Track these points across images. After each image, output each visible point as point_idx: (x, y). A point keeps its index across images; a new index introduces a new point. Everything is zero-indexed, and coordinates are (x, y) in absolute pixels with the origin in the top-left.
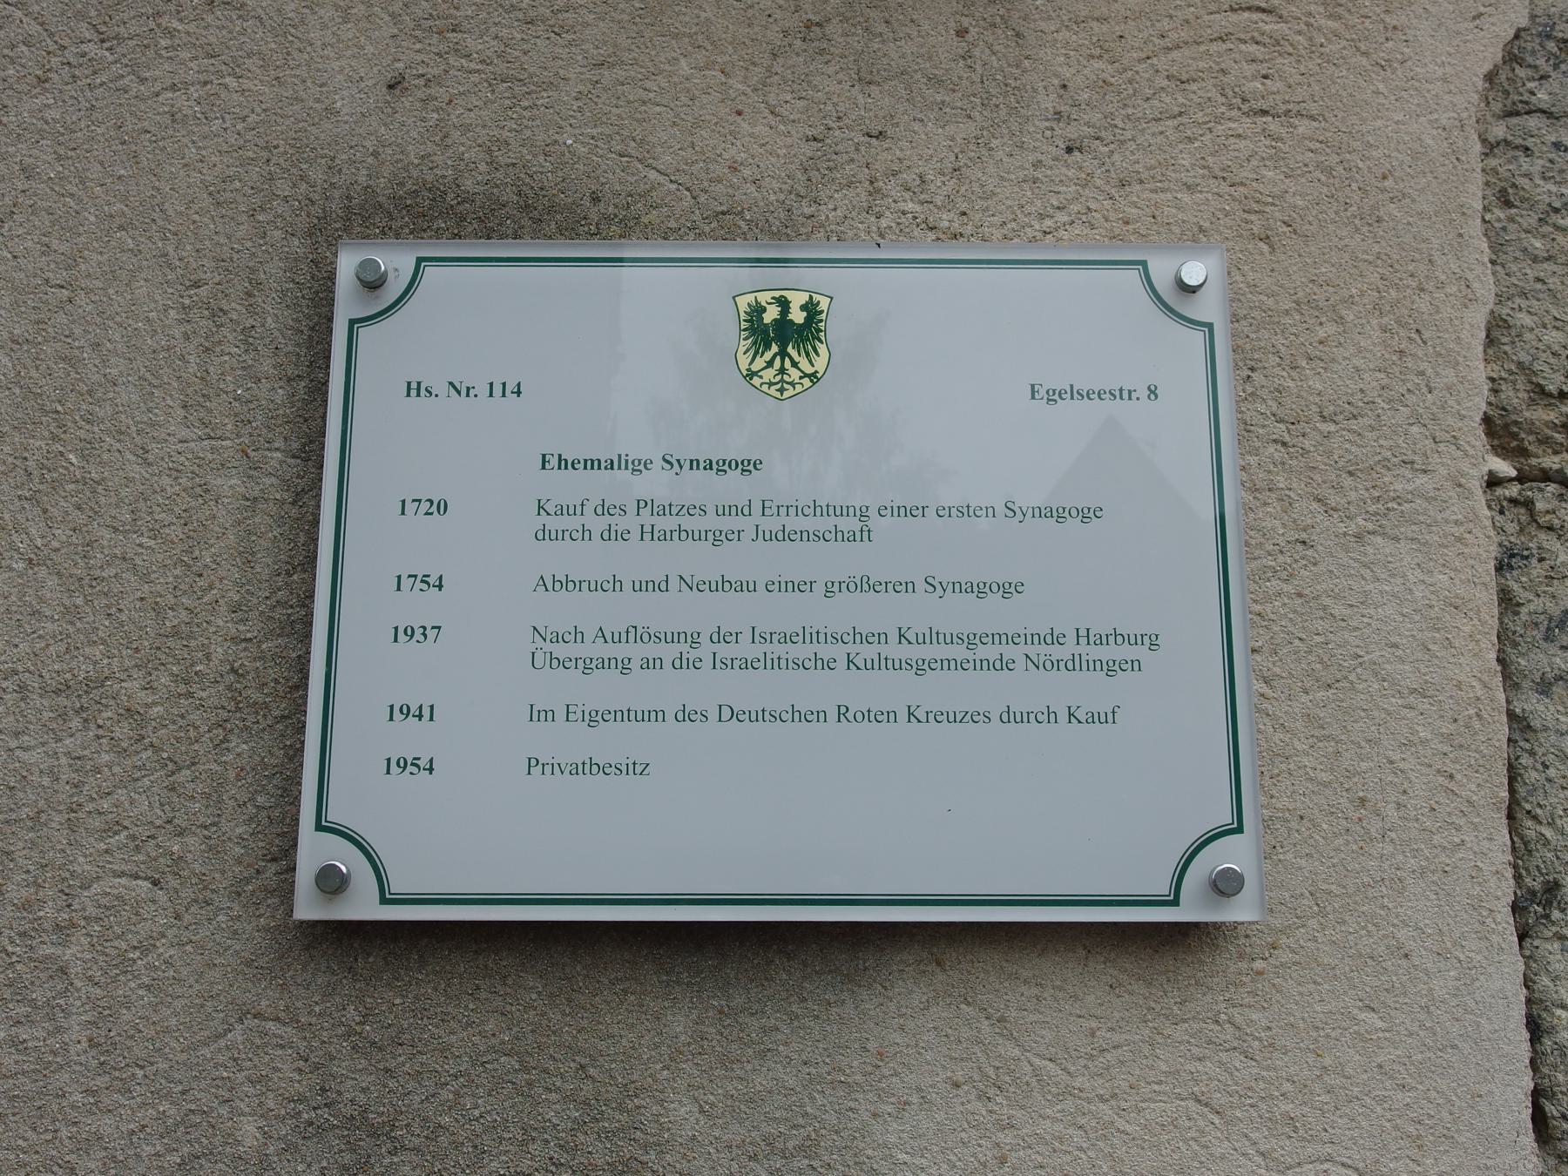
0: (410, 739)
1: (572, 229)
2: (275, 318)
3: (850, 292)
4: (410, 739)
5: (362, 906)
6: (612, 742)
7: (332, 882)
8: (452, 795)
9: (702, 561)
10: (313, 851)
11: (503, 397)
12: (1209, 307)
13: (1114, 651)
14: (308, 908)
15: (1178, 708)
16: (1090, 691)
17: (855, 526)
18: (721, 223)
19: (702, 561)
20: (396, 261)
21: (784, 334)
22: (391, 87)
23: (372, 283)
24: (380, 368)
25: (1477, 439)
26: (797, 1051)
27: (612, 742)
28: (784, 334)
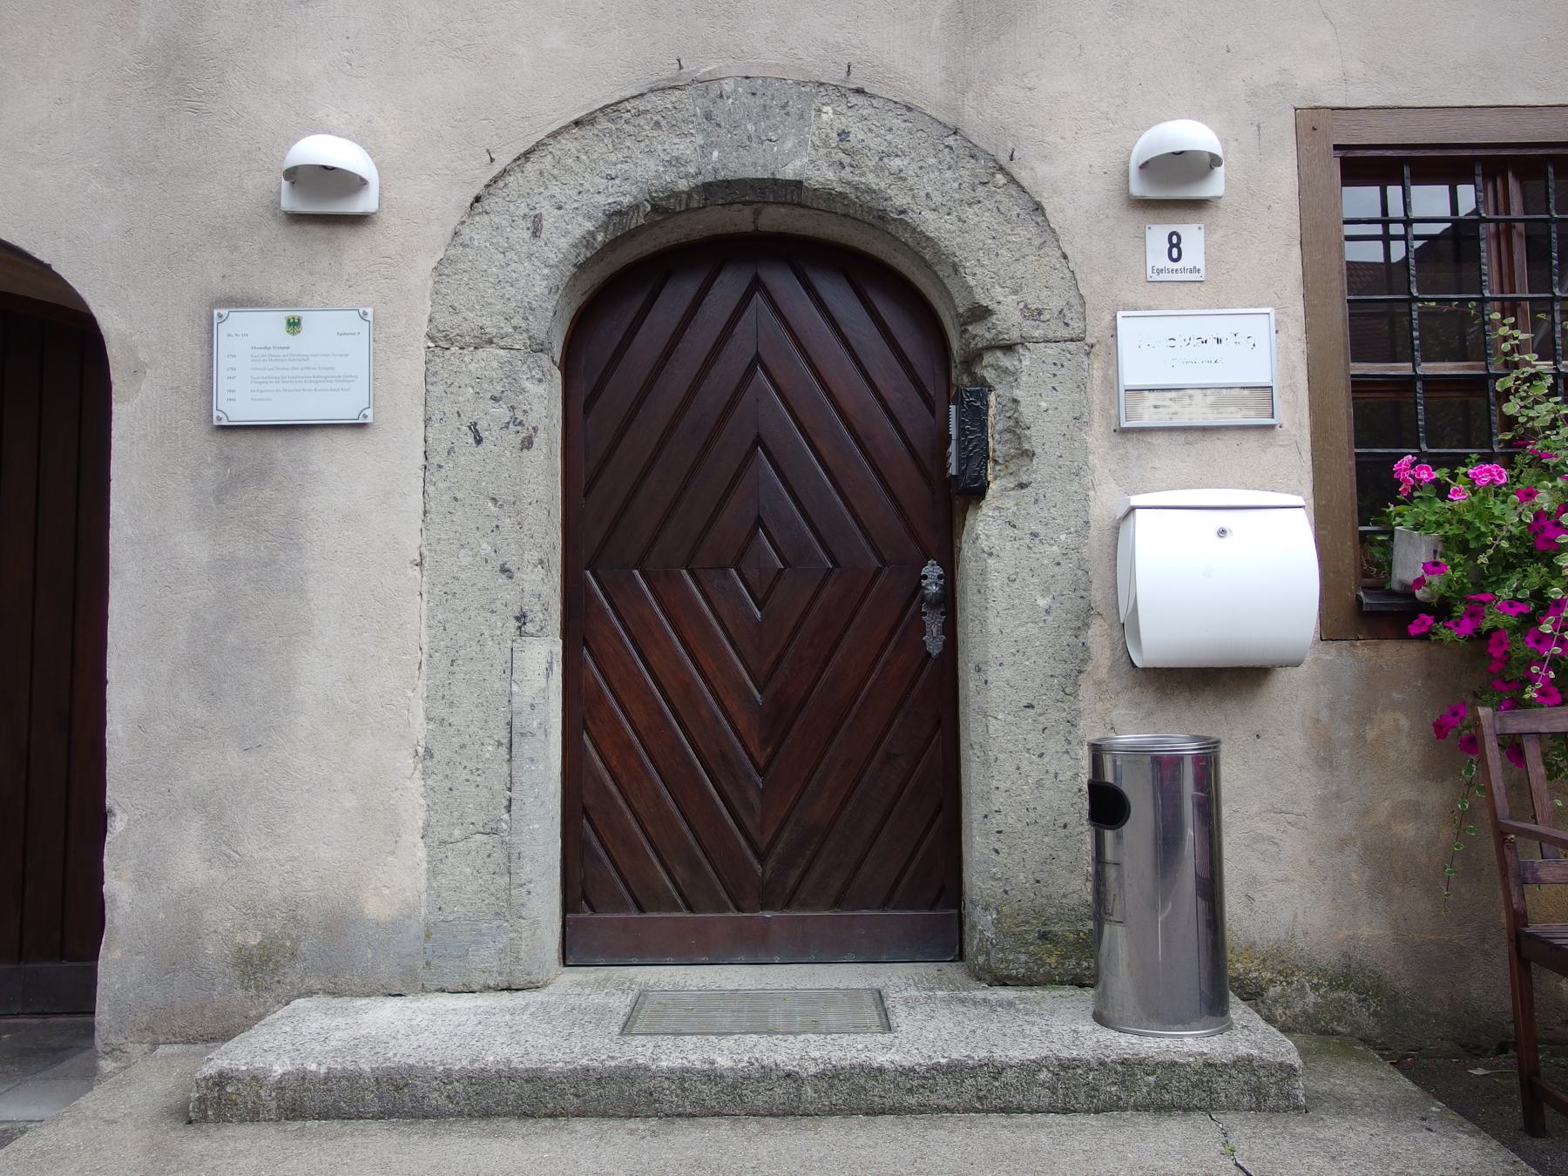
0: (231, 395)
1: (257, 305)
2: (204, 322)
3: (308, 318)
4: (231, 395)
5: (225, 423)
6: (265, 396)
7: (219, 419)
8: (237, 406)
9: (280, 365)
10: (216, 413)
11: (245, 336)
12: (370, 317)
13: (350, 379)
14: (216, 423)
15: (1203, 272)
16: (345, 386)
17: (306, 358)
18: (284, 304)
19: (280, 365)
20: (224, 312)
21: (294, 325)
22: (1043, 936)
23: (220, 316)
24: (222, 332)
25: (423, 339)
26: (299, 443)
27: (265, 396)
28: (294, 325)
